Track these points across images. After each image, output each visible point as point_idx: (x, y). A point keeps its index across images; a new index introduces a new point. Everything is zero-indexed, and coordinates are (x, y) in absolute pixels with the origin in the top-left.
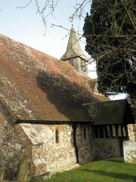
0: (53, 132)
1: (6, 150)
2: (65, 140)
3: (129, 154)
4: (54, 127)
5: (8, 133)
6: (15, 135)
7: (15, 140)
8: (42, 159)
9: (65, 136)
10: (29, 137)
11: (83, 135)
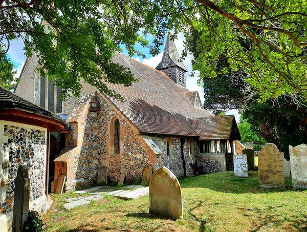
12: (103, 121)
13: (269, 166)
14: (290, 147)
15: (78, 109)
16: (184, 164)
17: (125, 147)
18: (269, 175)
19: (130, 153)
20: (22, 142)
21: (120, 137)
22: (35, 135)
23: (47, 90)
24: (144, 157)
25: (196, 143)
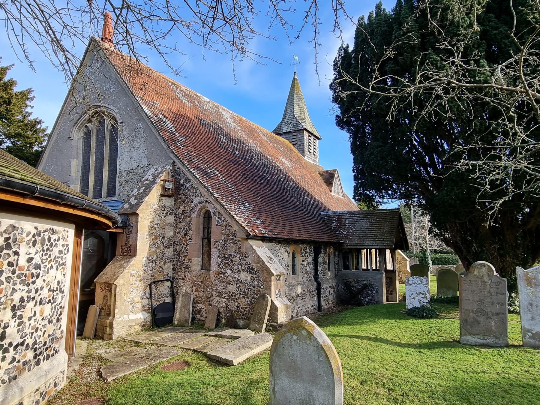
0: (289, 256)
1: (223, 282)
2: (304, 271)
3: (414, 298)
4: (290, 249)
5: (226, 256)
6: (240, 259)
7: (240, 267)
8: (283, 298)
9: (303, 263)
10: (266, 263)
11: (327, 264)
12: (183, 214)
13: (480, 302)
14: (519, 270)
15: (142, 190)
16: (319, 289)
17: (220, 260)
18: (478, 319)
19: (229, 272)
20: (10, 252)
21: (212, 243)
22: (43, 238)
23: (93, 158)
24: (253, 279)
25: (337, 253)
